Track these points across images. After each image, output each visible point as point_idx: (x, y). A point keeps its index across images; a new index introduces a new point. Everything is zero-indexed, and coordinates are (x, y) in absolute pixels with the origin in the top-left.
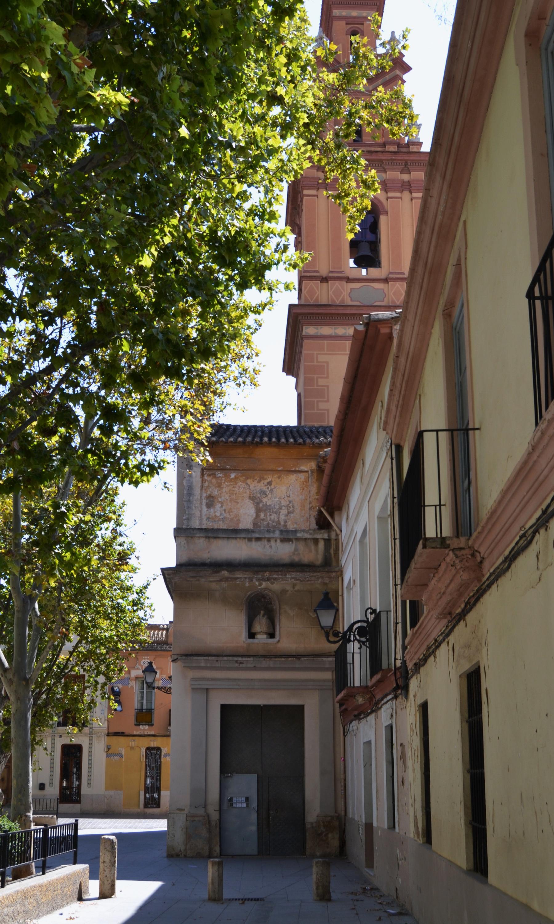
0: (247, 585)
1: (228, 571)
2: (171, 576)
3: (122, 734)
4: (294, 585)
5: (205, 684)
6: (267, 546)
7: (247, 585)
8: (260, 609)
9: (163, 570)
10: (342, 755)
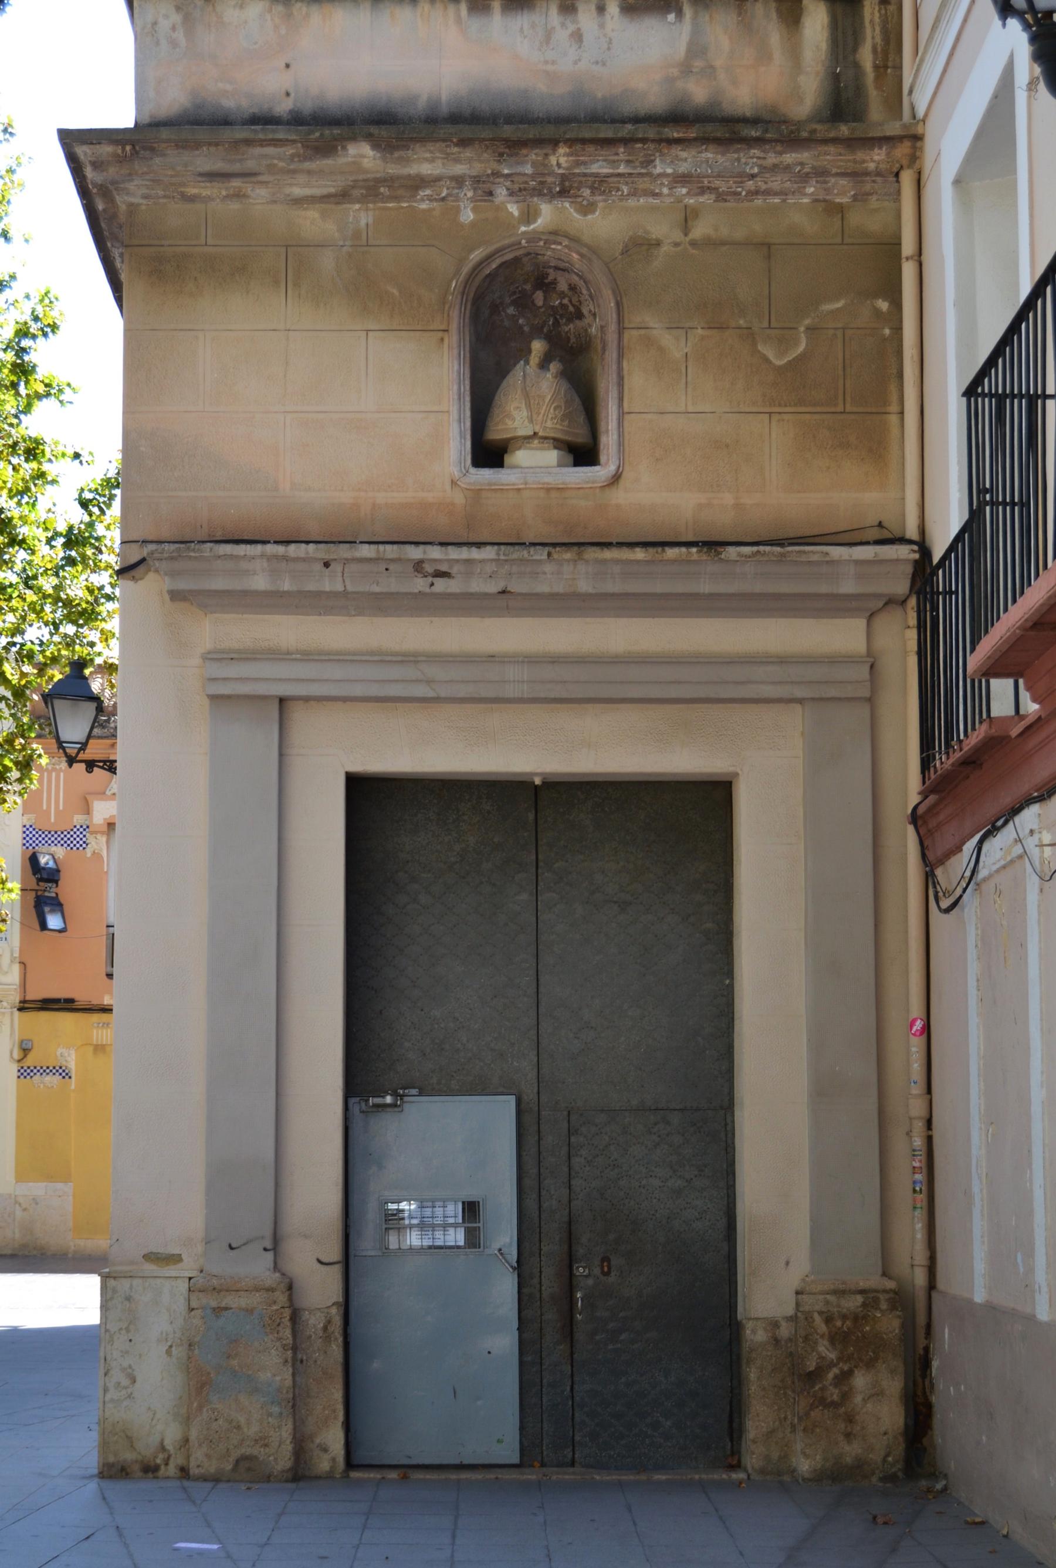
0: (468, 216)
1: (375, 146)
2: (112, 172)
3: (67, 1005)
4: (688, 218)
5: (276, 677)
6: (562, 35)
7: (468, 216)
8: (521, 323)
9: (72, 141)
10: (916, 1009)
